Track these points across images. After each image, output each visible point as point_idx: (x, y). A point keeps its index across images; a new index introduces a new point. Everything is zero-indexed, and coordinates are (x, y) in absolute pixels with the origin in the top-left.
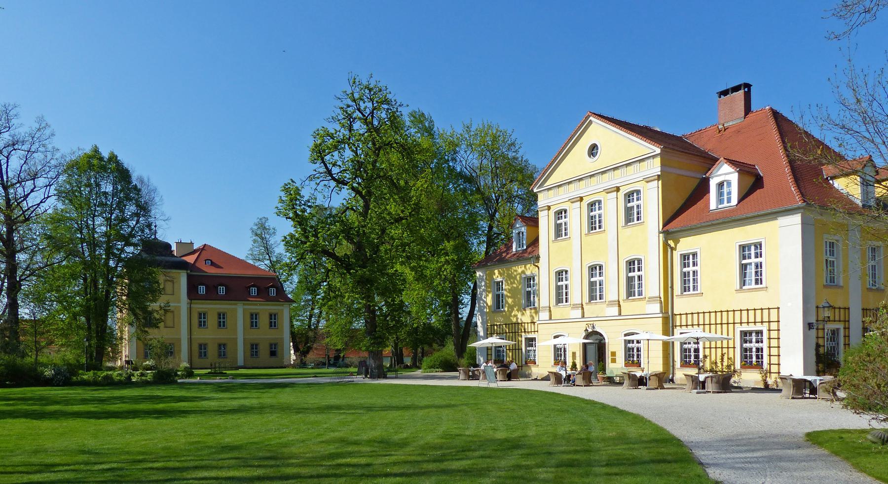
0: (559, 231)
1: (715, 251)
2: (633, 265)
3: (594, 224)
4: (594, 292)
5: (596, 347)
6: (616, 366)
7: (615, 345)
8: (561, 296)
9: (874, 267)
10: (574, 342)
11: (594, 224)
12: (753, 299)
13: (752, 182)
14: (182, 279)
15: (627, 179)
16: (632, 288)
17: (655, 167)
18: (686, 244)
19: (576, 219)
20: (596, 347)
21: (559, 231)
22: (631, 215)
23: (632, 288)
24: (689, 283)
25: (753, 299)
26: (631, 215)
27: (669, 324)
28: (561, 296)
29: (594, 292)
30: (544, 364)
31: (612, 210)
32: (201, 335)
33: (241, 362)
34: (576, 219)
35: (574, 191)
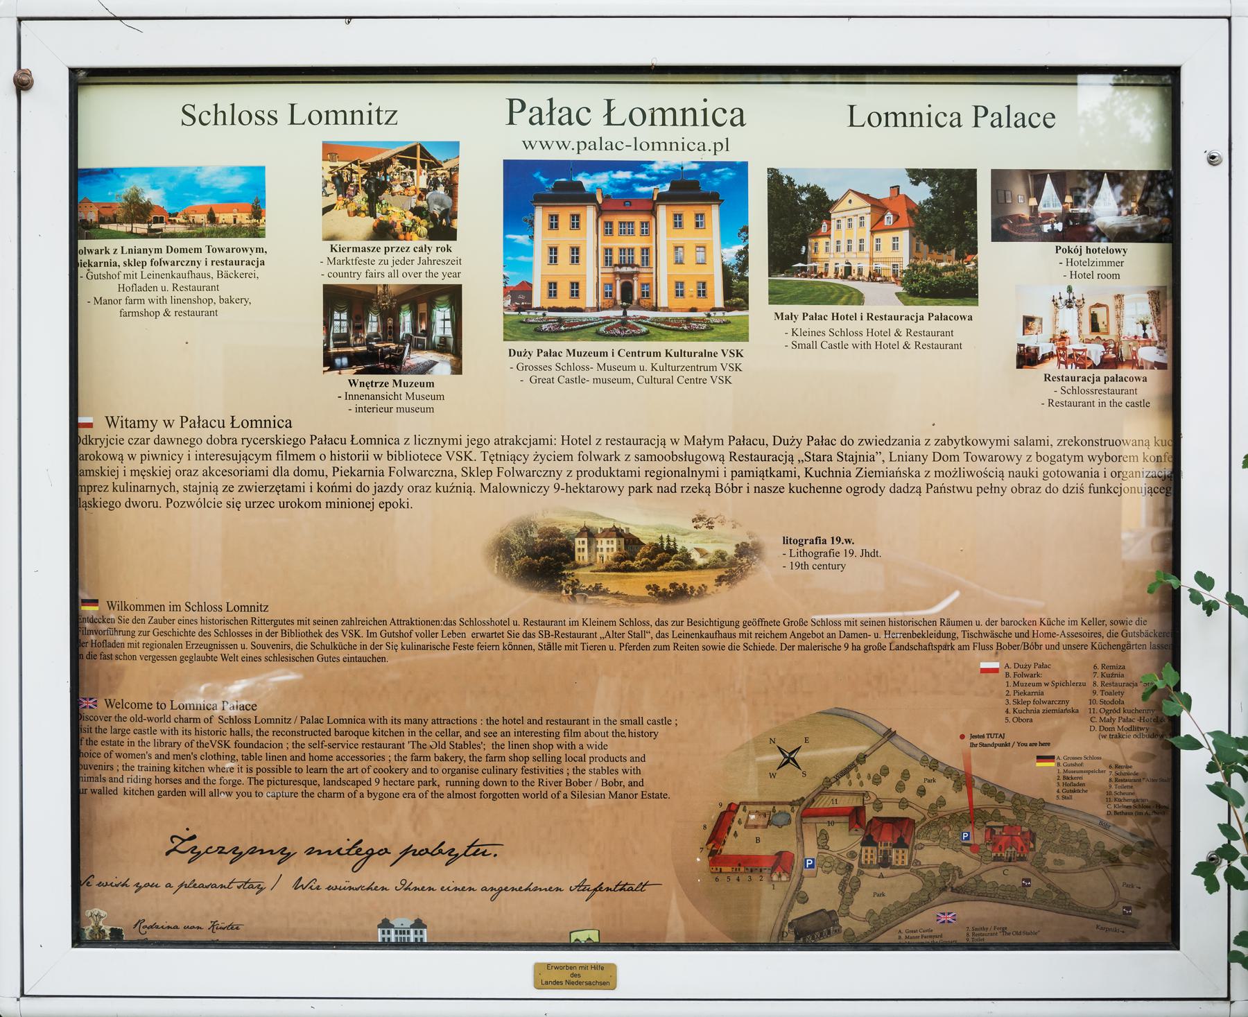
0: (839, 227)
1: (886, 238)
2: (861, 241)
3: (850, 226)
4: (849, 249)
5: (848, 270)
6: (855, 275)
7: (855, 267)
8: (838, 249)
9: (115, 264)
10: (842, 266)
11: (850, 226)
12: (896, 254)
13: (897, 217)
14: (741, 247)
15: (861, 212)
16: (861, 248)
17: (869, 210)
18: (877, 236)
19: (844, 223)
20: (848, 270)
21: (839, 227)
22: (862, 224)
23: (861, 248)
24: (878, 248)
25: (896, 254)
26: (862, 224)
27: (872, 259)
28: (838, 249)
29: (849, 249)
30: (831, 273)
31: (856, 222)
32: (554, 272)
33: (663, 302)
34: (844, 223)
35: (844, 214)
